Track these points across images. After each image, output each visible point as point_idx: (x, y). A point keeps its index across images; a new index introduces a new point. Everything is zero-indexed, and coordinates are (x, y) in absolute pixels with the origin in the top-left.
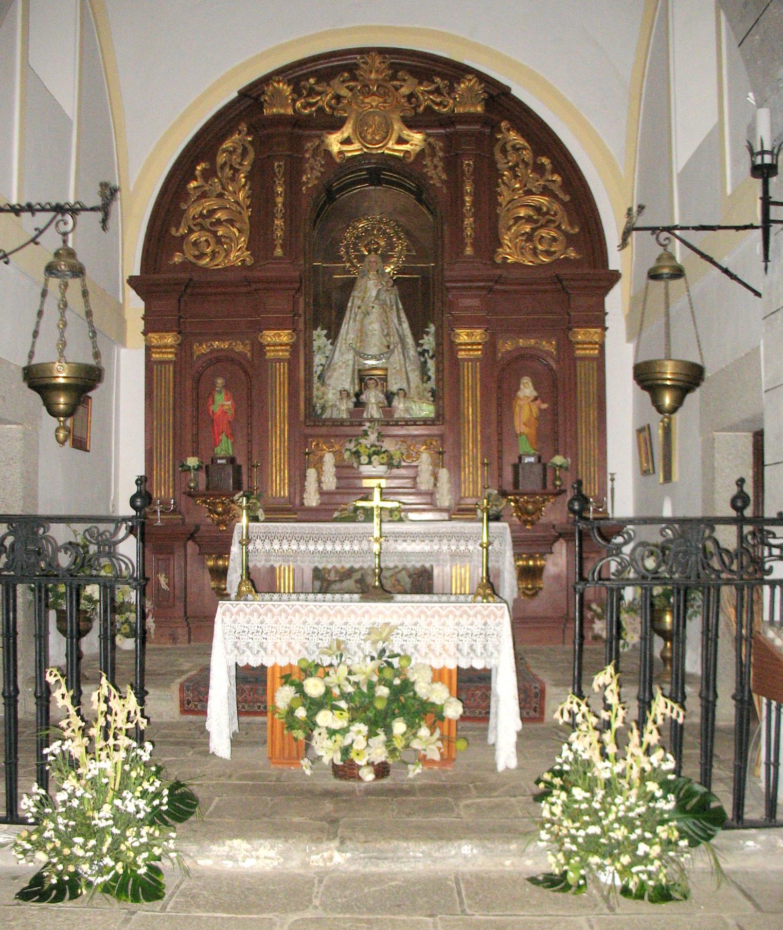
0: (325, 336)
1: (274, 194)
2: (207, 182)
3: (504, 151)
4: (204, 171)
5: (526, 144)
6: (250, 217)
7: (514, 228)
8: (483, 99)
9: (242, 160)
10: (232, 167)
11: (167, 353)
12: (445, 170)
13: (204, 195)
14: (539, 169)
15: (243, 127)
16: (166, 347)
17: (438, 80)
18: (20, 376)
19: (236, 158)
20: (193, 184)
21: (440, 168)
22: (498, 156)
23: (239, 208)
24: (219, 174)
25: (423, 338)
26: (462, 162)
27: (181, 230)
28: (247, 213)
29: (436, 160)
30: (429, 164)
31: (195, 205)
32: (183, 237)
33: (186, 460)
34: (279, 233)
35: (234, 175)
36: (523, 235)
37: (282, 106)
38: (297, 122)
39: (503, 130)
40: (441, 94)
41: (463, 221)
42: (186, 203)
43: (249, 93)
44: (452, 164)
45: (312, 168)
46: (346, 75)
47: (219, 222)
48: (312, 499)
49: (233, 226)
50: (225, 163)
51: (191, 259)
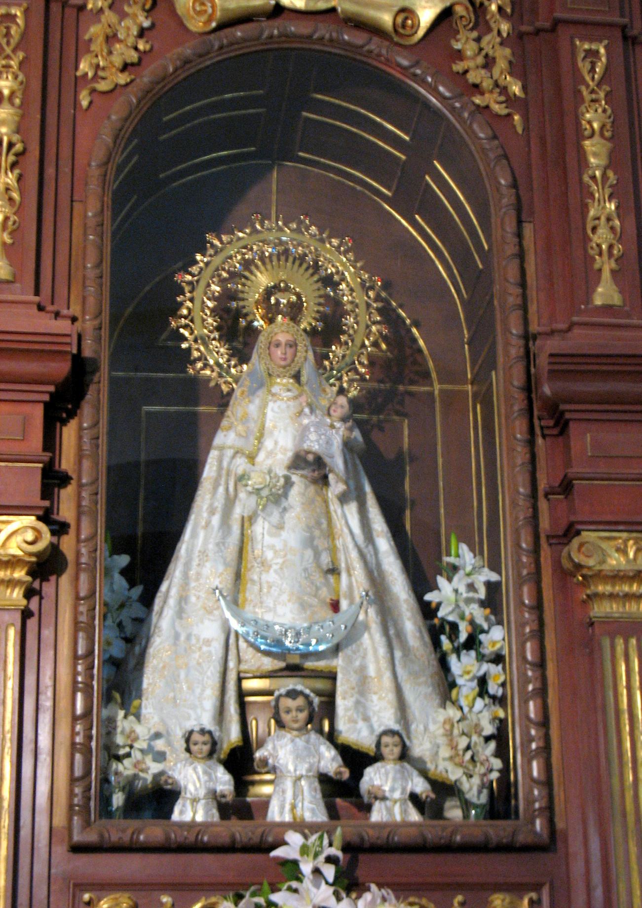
0: (124, 572)
12: (517, 69)
18: (71, 854)
21: (501, 65)
25: (435, 587)
26: (573, 49)
30: (470, 49)
41: (585, 209)
45: (111, 39)
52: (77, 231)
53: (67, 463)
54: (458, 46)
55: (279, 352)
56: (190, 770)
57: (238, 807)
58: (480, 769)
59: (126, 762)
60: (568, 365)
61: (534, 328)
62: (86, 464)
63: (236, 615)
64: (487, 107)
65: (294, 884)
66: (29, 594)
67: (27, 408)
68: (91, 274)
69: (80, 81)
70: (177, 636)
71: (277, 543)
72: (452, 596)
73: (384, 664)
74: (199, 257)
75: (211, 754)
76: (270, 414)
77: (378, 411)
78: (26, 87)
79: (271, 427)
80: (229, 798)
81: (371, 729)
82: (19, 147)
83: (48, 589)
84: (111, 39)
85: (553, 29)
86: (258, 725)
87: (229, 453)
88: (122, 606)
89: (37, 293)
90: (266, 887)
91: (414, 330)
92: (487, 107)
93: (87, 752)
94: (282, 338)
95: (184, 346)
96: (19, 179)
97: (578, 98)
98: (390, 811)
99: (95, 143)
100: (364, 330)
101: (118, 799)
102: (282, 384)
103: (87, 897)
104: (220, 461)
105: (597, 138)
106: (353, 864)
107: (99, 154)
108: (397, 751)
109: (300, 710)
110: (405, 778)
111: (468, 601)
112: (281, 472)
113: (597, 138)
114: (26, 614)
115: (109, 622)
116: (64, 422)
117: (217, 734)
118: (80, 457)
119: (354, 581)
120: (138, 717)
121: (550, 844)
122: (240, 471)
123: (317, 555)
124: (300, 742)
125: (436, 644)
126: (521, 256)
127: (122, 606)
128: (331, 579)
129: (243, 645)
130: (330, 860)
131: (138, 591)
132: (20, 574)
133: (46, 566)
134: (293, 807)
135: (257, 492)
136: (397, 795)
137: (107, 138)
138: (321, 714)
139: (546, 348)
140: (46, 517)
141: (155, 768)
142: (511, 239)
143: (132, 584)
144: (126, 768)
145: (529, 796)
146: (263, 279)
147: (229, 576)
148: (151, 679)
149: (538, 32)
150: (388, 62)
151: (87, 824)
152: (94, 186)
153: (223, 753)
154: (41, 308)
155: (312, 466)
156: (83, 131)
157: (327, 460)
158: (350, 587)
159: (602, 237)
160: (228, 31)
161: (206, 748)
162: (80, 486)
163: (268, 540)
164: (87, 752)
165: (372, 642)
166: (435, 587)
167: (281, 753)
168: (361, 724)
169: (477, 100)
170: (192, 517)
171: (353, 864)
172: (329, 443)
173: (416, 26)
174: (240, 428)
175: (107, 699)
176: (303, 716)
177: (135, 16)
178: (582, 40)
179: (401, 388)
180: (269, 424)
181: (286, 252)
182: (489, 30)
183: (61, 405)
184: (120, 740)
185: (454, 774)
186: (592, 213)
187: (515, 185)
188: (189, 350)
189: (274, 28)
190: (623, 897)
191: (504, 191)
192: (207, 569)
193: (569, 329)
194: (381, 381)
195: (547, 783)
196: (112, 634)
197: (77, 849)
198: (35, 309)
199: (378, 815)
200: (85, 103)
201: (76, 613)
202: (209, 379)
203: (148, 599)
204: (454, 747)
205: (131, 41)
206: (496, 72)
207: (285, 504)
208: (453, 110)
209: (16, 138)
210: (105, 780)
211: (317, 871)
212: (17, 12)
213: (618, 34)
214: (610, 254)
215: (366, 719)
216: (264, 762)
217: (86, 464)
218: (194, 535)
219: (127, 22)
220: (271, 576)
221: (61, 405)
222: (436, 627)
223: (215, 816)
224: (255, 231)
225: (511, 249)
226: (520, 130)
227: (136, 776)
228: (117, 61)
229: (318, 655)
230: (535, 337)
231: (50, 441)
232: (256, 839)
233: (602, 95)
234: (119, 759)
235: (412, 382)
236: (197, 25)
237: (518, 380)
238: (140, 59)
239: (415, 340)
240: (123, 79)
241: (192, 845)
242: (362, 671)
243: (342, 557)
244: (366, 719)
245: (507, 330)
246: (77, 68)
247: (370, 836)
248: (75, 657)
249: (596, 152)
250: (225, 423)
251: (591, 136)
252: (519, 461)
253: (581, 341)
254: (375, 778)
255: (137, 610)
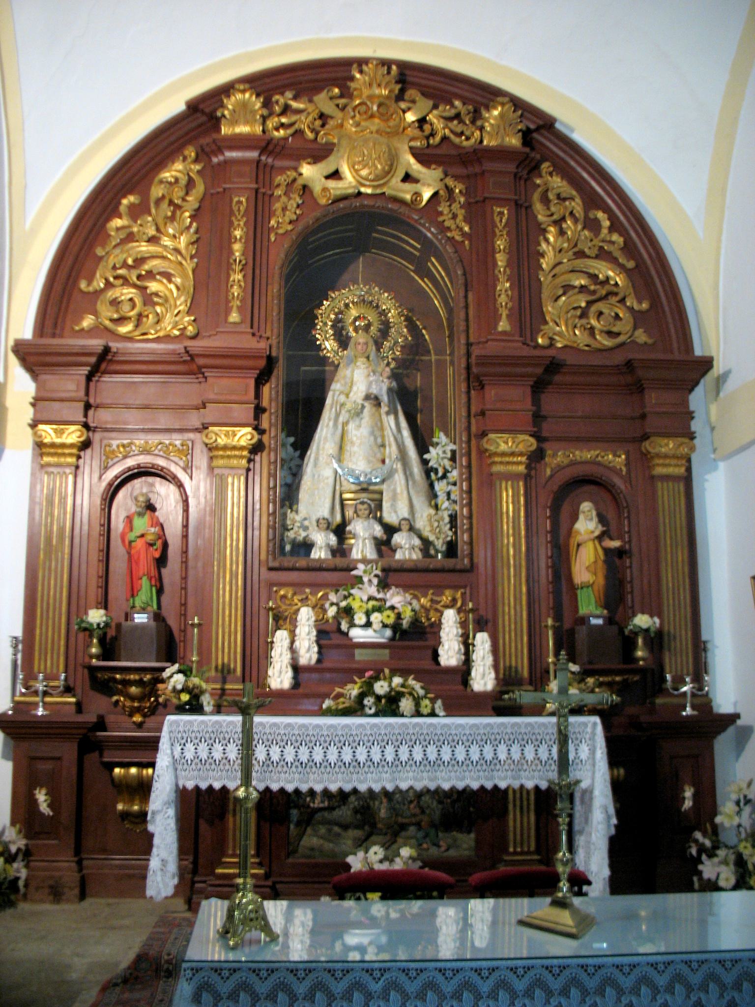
1: (231, 239)
2: (136, 222)
3: (545, 200)
4: (131, 207)
5: (574, 193)
6: (194, 271)
7: (563, 298)
8: (520, 131)
9: (187, 194)
10: (171, 202)
11: (64, 455)
13: (130, 237)
14: (592, 225)
15: (191, 152)
16: (63, 446)
17: (457, 103)
19: (177, 194)
20: (117, 222)
21: (460, 217)
22: (538, 207)
23: (179, 258)
24: (153, 211)
25: (428, 452)
26: (492, 212)
27: (95, 283)
28: (189, 266)
29: (455, 207)
31: (117, 251)
32: (98, 293)
33: (86, 613)
34: (236, 291)
35: (174, 213)
36: (575, 308)
37: (246, 123)
38: (267, 146)
39: (544, 174)
40: (461, 121)
41: (495, 287)
42: (103, 247)
43: (201, 106)
44: (477, 209)
45: (284, 209)
46: (336, 90)
47: (151, 275)
48: (279, 677)
49: (170, 281)
50: (163, 197)
51: (107, 323)
52: (269, 298)
53: (265, 403)
54: (440, 209)
55: (360, 347)
56: (318, 535)
57: (340, 550)
58: (443, 536)
59: (292, 532)
60: (484, 361)
61: (472, 340)
62: (273, 404)
63: (340, 467)
64: (453, 238)
65: (360, 586)
66: (250, 461)
67: (248, 380)
68: (275, 319)
69: (270, 230)
70: (314, 476)
71: (358, 433)
72: (436, 456)
73: (404, 487)
74: (325, 302)
75: (328, 528)
76: (355, 376)
77: (407, 368)
78: (247, 234)
79: (357, 381)
80: (335, 547)
81: (398, 517)
82: (244, 262)
83: (258, 458)
84: (284, 209)
85: (484, 201)
86: (349, 513)
87: (337, 393)
88: (291, 460)
89: (252, 328)
90: (349, 586)
91: (424, 331)
92: (453, 238)
93: (274, 528)
94: (361, 340)
95: (318, 343)
96: (244, 276)
97: (494, 234)
98: (404, 554)
99: (277, 256)
100: (400, 334)
101: (288, 548)
102: (361, 362)
103: (275, 589)
104: (333, 396)
105: (502, 252)
106: (386, 577)
107: (279, 263)
108: (408, 527)
109: (365, 510)
110: (410, 538)
111: (443, 458)
112: (360, 401)
113: (502, 252)
114: (248, 470)
115: (285, 467)
116: (264, 385)
117: (330, 520)
118: (271, 400)
119: (392, 450)
120: (297, 512)
121: (472, 568)
122: (342, 401)
123: (376, 439)
124: (366, 523)
125: (428, 476)
126: (467, 307)
127: (291, 460)
128: (382, 449)
129: (342, 478)
130: (376, 576)
131: (298, 453)
132: (245, 453)
133: (257, 449)
134: (362, 551)
135: (349, 411)
136: (407, 546)
137: (282, 256)
138: (375, 509)
139: (476, 351)
140: (256, 428)
141: (303, 534)
142: (462, 300)
143: (295, 449)
144: (291, 534)
145: (463, 548)
146: (354, 312)
147: (336, 448)
148: (303, 495)
149: (477, 202)
150: (408, 217)
151: (275, 558)
152: (277, 277)
153: (334, 527)
154: (254, 335)
155: (376, 401)
156: (273, 252)
157: (380, 397)
158: (390, 453)
159: (503, 299)
160: (337, 204)
161: (325, 526)
162: (271, 414)
163: (354, 432)
164: (274, 528)
165: (399, 478)
166: (428, 452)
167: (357, 528)
168: (393, 514)
169: (449, 234)
170: (321, 422)
171: (386, 577)
172: (381, 389)
173: (421, 201)
174: (343, 382)
175: (282, 506)
176: (367, 512)
177: (295, 199)
178: (497, 206)
179: (417, 358)
180: (355, 379)
181: (364, 301)
182: (455, 201)
183: (262, 378)
184: (288, 522)
185: (432, 538)
186: (498, 288)
187: (465, 274)
188: (320, 345)
189: (357, 203)
190: (500, 592)
191: (460, 277)
192: (328, 445)
193: (487, 342)
194: (408, 355)
195: (471, 543)
196: (285, 473)
197: (271, 569)
198: (250, 336)
199: (398, 556)
200: (273, 239)
201: (269, 469)
202: (329, 357)
203: (302, 456)
204: (432, 526)
205: (293, 210)
206: (458, 221)
207: (361, 416)
208: (437, 238)
209: (242, 258)
210: (282, 540)
211: (370, 581)
212: (243, 199)
213: (513, 204)
214: (506, 307)
215: (396, 512)
216: (350, 532)
217: (273, 404)
218: (322, 430)
219: (292, 202)
220: (355, 449)
221: (262, 378)
222: (428, 471)
223: (330, 557)
224: (350, 290)
225: (462, 304)
226: (468, 248)
227: (295, 538)
228: (287, 220)
229: (376, 484)
230: (472, 344)
231: (258, 395)
232: (345, 566)
233: (505, 233)
234: (288, 530)
235: (422, 355)
236: (323, 201)
237: (463, 365)
238: (297, 219)
239: (423, 335)
240: (290, 227)
241: (319, 567)
242: (394, 491)
243: (387, 439)
244: (396, 512)
245: (459, 341)
246: (269, 223)
247: (394, 565)
248: (269, 488)
249: (501, 260)
250: (336, 379)
251: (500, 251)
252: (463, 401)
253: (492, 348)
254: (398, 538)
255: (297, 461)
